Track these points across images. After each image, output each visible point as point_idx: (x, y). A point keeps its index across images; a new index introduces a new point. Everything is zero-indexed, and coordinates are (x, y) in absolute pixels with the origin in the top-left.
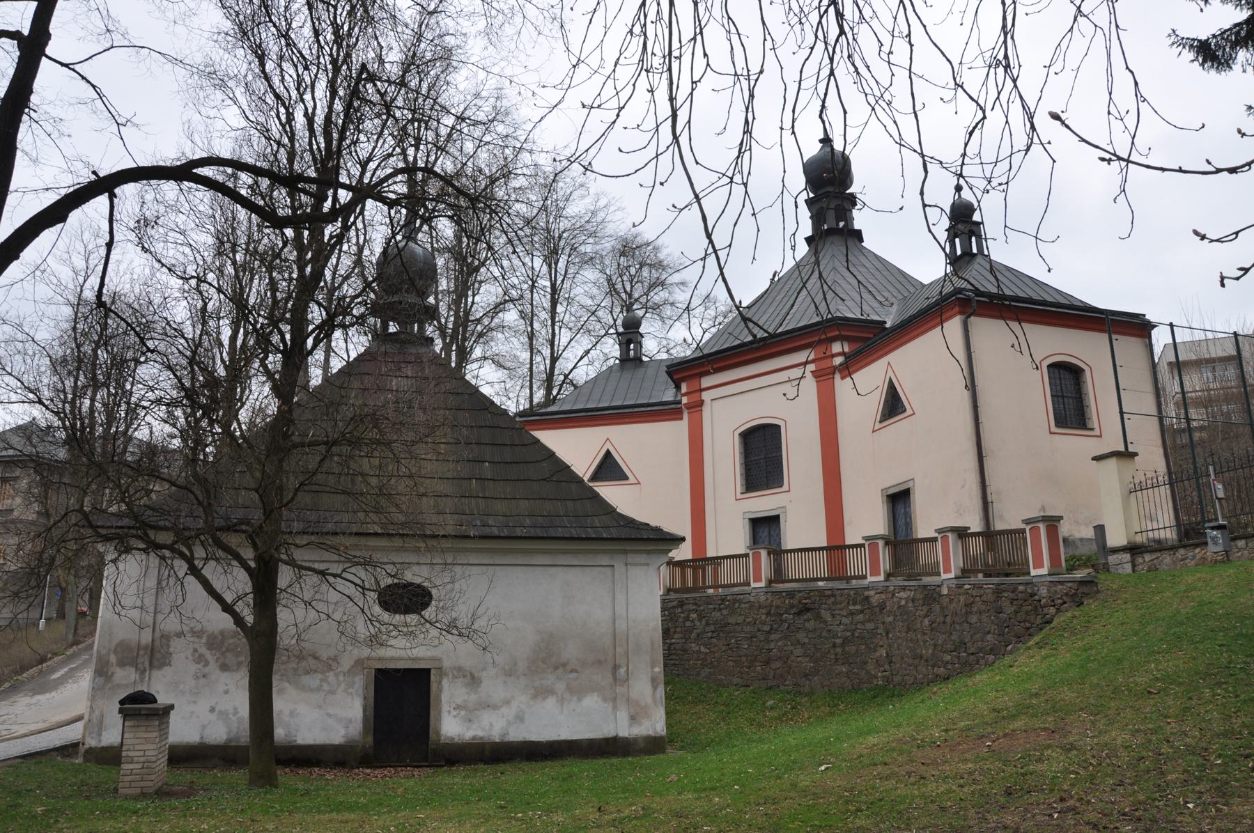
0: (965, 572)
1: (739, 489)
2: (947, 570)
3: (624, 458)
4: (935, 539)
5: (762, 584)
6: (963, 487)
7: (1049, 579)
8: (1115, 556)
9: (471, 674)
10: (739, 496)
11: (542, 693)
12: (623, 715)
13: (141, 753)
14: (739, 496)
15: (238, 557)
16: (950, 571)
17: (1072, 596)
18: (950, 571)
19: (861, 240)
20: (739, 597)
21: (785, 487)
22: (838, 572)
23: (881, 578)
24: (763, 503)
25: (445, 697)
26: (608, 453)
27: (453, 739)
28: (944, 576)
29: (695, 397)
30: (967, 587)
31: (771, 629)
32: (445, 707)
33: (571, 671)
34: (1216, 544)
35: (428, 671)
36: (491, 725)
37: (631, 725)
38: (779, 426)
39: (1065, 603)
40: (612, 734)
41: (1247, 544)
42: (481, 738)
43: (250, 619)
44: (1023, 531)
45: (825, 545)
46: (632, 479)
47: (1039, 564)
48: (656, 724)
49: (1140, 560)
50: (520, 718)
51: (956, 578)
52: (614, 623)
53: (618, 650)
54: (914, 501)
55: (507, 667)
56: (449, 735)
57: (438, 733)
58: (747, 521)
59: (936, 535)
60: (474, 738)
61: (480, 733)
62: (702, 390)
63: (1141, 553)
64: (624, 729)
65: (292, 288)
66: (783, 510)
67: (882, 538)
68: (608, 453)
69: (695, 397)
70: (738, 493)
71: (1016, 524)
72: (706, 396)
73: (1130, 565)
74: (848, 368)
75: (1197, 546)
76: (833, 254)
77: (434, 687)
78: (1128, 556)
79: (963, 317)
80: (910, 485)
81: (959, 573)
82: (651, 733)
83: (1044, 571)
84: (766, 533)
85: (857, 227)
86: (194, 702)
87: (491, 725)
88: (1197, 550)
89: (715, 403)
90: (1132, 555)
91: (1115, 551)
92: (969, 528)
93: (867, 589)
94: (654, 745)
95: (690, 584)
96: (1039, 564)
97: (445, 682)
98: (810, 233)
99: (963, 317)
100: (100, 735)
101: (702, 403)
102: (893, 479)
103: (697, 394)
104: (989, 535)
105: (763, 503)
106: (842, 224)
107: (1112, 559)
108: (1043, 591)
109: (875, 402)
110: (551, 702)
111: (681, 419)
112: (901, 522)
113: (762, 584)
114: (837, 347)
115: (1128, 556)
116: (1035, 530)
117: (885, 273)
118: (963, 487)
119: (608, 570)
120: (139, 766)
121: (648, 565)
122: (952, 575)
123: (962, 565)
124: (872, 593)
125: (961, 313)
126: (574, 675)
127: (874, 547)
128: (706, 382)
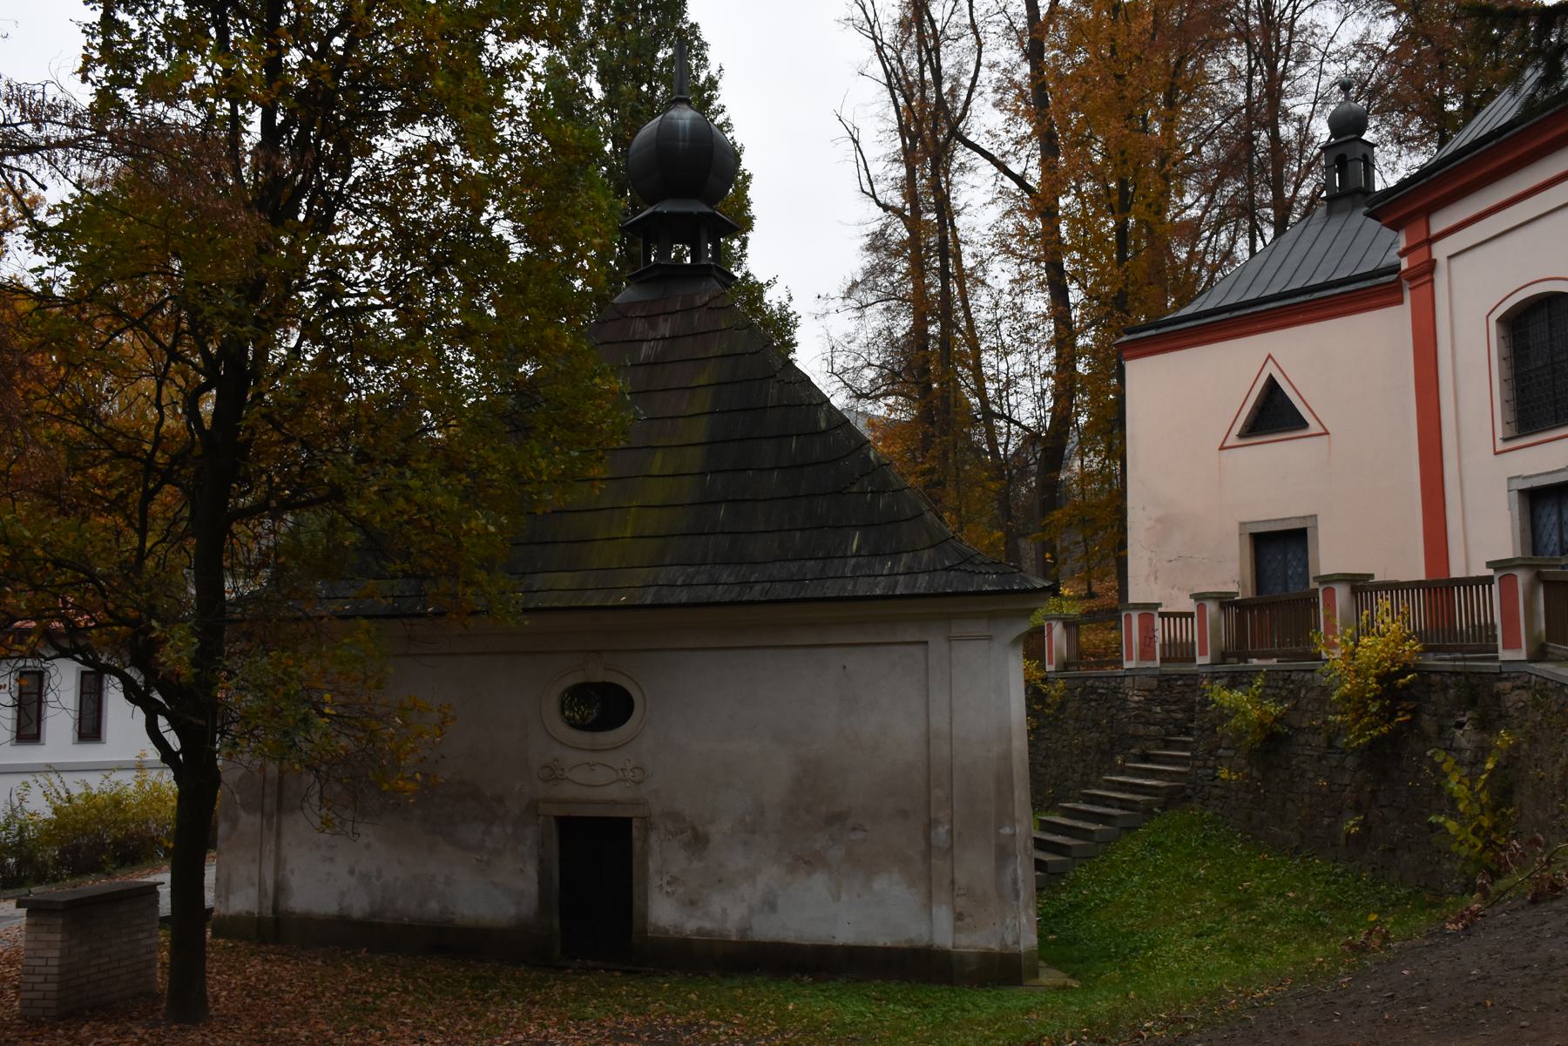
3: (1303, 390)
9: (694, 829)
11: (808, 862)
13: (43, 962)
14: (1500, 446)
22: (1438, 636)
25: (653, 864)
26: (1272, 385)
27: (667, 931)
29: (1420, 256)
32: (655, 881)
33: (854, 829)
35: (629, 820)
36: (724, 911)
37: (956, 930)
40: (923, 941)
42: (709, 933)
46: (1314, 427)
50: (770, 905)
52: (928, 744)
55: (748, 818)
56: (661, 924)
57: (645, 916)
58: (1515, 495)
59: (1491, 572)
60: (699, 931)
61: (708, 925)
62: (1431, 241)
64: (942, 932)
65: (1256, 93)
67: (1215, 598)
68: (1272, 385)
69: (1420, 256)
70: (1498, 441)
71: (1481, 570)
72: (1440, 251)
77: (637, 844)
82: (995, 946)
84: (1554, 518)
86: (332, 860)
87: (724, 911)
89: (1456, 262)
92: (1371, 576)
93: (1499, 676)
95: (1179, 656)
97: (654, 839)
100: (227, 899)
101: (1431, 266)
103: (1423, 252)
104: (88, 795)
110: (819, 881)
111: (1400, 302)
119: (917, 651)
120: (41, 979)
121: (990, 638)
124: (1508, 685)
126: (858, 835)
127: (1508, 584)
128: (1439, 223)
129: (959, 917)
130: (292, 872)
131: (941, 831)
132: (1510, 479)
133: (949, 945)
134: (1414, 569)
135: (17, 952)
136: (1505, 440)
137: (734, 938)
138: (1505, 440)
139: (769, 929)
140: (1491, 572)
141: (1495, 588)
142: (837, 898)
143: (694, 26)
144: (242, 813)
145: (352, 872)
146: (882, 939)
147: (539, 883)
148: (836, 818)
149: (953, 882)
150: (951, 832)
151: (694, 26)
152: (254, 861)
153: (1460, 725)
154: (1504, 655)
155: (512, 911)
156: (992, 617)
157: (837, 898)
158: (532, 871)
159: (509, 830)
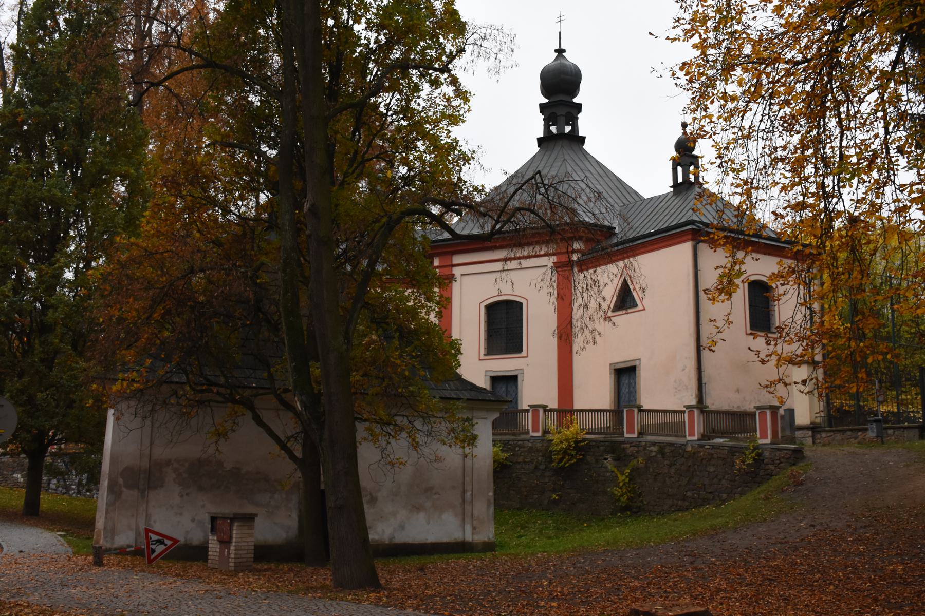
0: (704, 437)
1: (483, 351)
2: (692, 434)
4: (684, 412)
5: (539, 434)
6: (684, 370)
7: (770, 446)
8: (800, 432)
9: (371, 494)
10: (482, 357)
12: (468, 528)
15: (290, 407)
16: (694, 435)
17: (787, 459)
18: (694, 435)
19: (583, 143)
20: (520, 442)
21: (524, 353)
23: (635, 435)
24: (504, 365)
28: (689, 438)
30: (707, 447)
31: (546, 468)
33: (435, 494)
34: (873, 431)
36: (383, 531)
37: (473, 534)
38: (521, 304)
39: (781, 463)
41: (894, 432)
42: (377, 541)
43: (298, 454)
44: (753, 415)
45: (609, 408)
47: (764, 436)
48: (487, 533)
49: (818, 436)
50: (402, 527)
51: (698, 440)
53: (467, 479)
54: (640, 376)
58: (488, 378)
59: (685, 409)
63: (820, 431)
66: (521, 372)
72: (457, 271)
73: (811, 439)
74: (583, 265)
75: (860, 430)
76: (562, 152)
78: (810, 433)
79: (694, 243)
80: (637, 363)
81: (700, 437)
82: (486, 539)
83: (768, 441)
85: (581, 134)
86: (181, 514)
88: (860, 433)
89: (465, 278)
90: (813, 432)
91: (801, 428)
92: (547, 406)
93: (623, 443)
94: (489, 547)
96: (764, 436)
98: (541, 135)
99: (694, 243)
101: (451, 278)
102: (622, 357)
105: (504, 365)
106: (568, 129)
107: (798, 434)
108: (766, 454)
109: (610, 292)
110: (422, 516)
112: (625, 390)
113: (539, 434)
114: (577, 246)
115: (810, 433)
116: (763, 414)
117: (606, 179)
118: (684, 370)
121: (486, 418)
122: (696, 438)
123: (702, 431)
124: (628, 445)
125: (692, 240)
126: (436, 497)
128: (457, 259)
129: (474, 528)
130: (155, 522)
131: (468, 494)
132: (486, 371)
133: (470, 540)
134: (577, 405)
135: (563, 534)
136: (485, 355)
137: (387, 542)
138: (485, 355)
139: (402, 538)
140: (685, 409)
141: (530, 414)
142: (428, 523)
143: (579, 107)
144: (125, 490)
145: (193, 520)
146: (445, 539)
147: (299, 522)
148: (429, 490)
149: (472, 515)
150: (472, 495)
151: (579, 107)
152: (133, 516)
153: (606, 459)
154: (626, 435)
155: (284, 535)
156: (488, 410)
157: (428, 523)
158: (295, 515)
159: (284, 496)
